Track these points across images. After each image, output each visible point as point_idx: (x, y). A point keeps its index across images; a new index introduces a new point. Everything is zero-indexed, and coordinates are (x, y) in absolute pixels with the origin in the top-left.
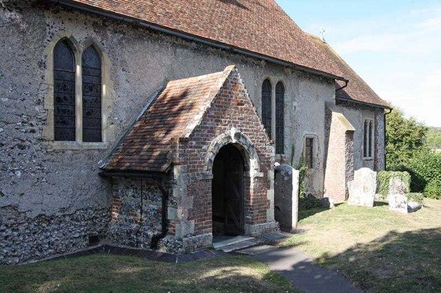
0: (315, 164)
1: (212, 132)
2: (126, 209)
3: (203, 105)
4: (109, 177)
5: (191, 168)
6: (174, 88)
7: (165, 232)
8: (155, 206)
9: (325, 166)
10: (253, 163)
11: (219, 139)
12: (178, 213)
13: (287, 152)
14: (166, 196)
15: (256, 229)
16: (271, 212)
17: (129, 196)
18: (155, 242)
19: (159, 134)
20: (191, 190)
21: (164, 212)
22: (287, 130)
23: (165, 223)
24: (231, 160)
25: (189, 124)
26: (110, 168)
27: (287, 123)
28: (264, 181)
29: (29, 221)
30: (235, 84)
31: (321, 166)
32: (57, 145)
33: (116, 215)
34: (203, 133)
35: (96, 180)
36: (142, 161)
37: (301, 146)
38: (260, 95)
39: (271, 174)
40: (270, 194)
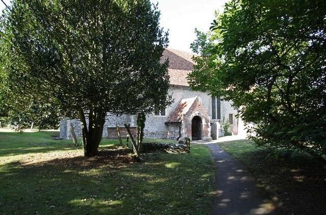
0: (234, 123)
1: (191, 113)
2: (171, 132)
3: (189, 106)
4: (167, 124)
5: (186, 120)
6: (183, 101)
7: (180, 137)
8: (177, 131)
9: (238, 123)
10: (204, 121)
11: (193, 115)
12: (183, 131)
13: (222, 119)
14: (180, 128)
15: (204, 138)
16: (209, 134)
17: (172, 129)
18: (178, 138)
19: (179, 113)
20: (186, 127)
21: (180, 132)
22: (221, 111)
23: (180, 135)
24: (197, 120)
25: (185, 110)
26: (267, 212)
27: (221, 109)
28: (207, 126)
29: (150, 134)
30: (198, 100)
31: (236, 123)
32: (155, 116)
33: (169, 134)
34: (188, 113)
35: (164, 125)
36: (175, 120)
37: (227, 117)
38: (211, 101)
39: (209, 124)
40: (209, 129)
